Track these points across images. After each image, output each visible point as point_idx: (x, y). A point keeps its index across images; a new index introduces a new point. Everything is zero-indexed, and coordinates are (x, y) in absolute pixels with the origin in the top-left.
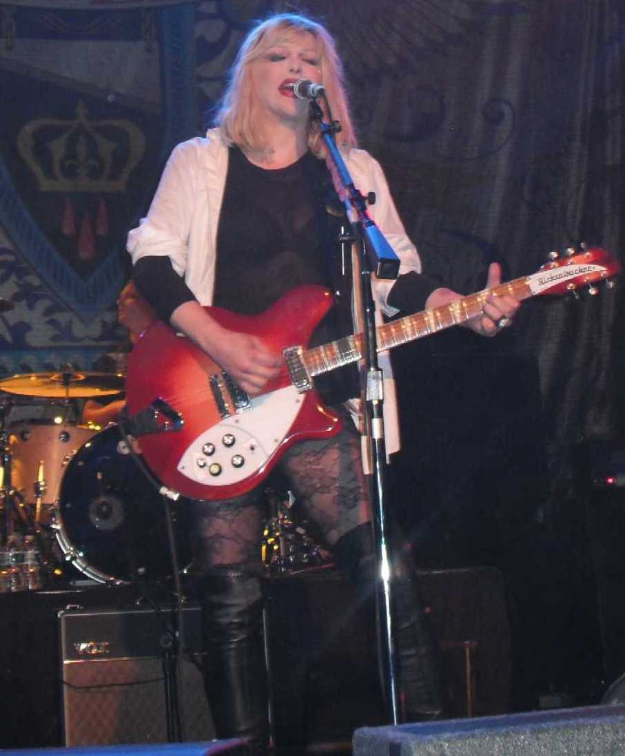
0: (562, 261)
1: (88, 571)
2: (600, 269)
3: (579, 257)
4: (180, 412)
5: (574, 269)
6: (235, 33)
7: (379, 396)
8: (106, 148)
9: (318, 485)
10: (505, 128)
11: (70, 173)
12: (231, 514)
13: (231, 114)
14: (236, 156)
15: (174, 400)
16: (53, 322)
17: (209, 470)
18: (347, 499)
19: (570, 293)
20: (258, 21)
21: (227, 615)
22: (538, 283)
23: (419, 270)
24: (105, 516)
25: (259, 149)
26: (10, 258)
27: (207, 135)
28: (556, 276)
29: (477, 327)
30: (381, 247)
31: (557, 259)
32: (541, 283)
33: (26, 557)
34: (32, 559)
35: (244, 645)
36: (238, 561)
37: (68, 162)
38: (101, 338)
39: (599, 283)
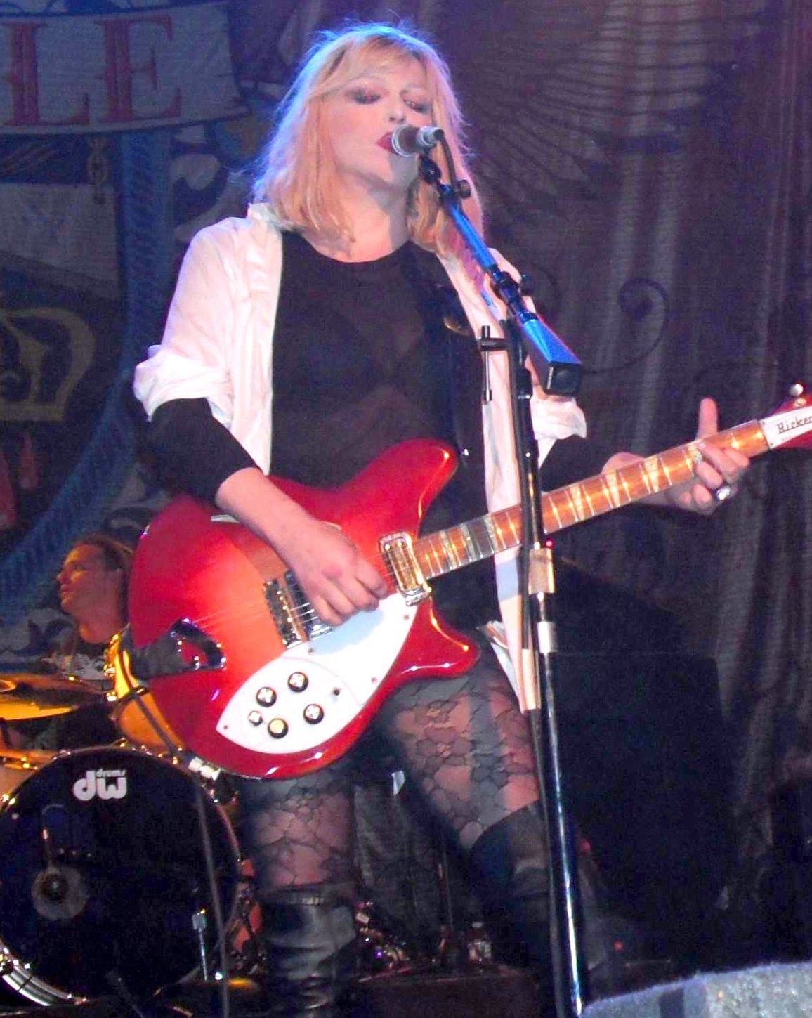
1: (27, 990)
6: (235, 176)
7: (547, 587)
8: (32, 351)
9: (446, 754)
10: (655, 321)
12: (306, 805)
13: (287, 178)
15: (214, 619)
17: (269, 728)
20: (328, 33)
21: (304, 965)
23: (583, 433)
24: (56, 898)
25: (332, 235)
27: (250, 212)
28: (805, 420)
29: (685, 500)
30: (550, 347)
32: (782, 430)
36: (320, 879)
38: (28, 651)
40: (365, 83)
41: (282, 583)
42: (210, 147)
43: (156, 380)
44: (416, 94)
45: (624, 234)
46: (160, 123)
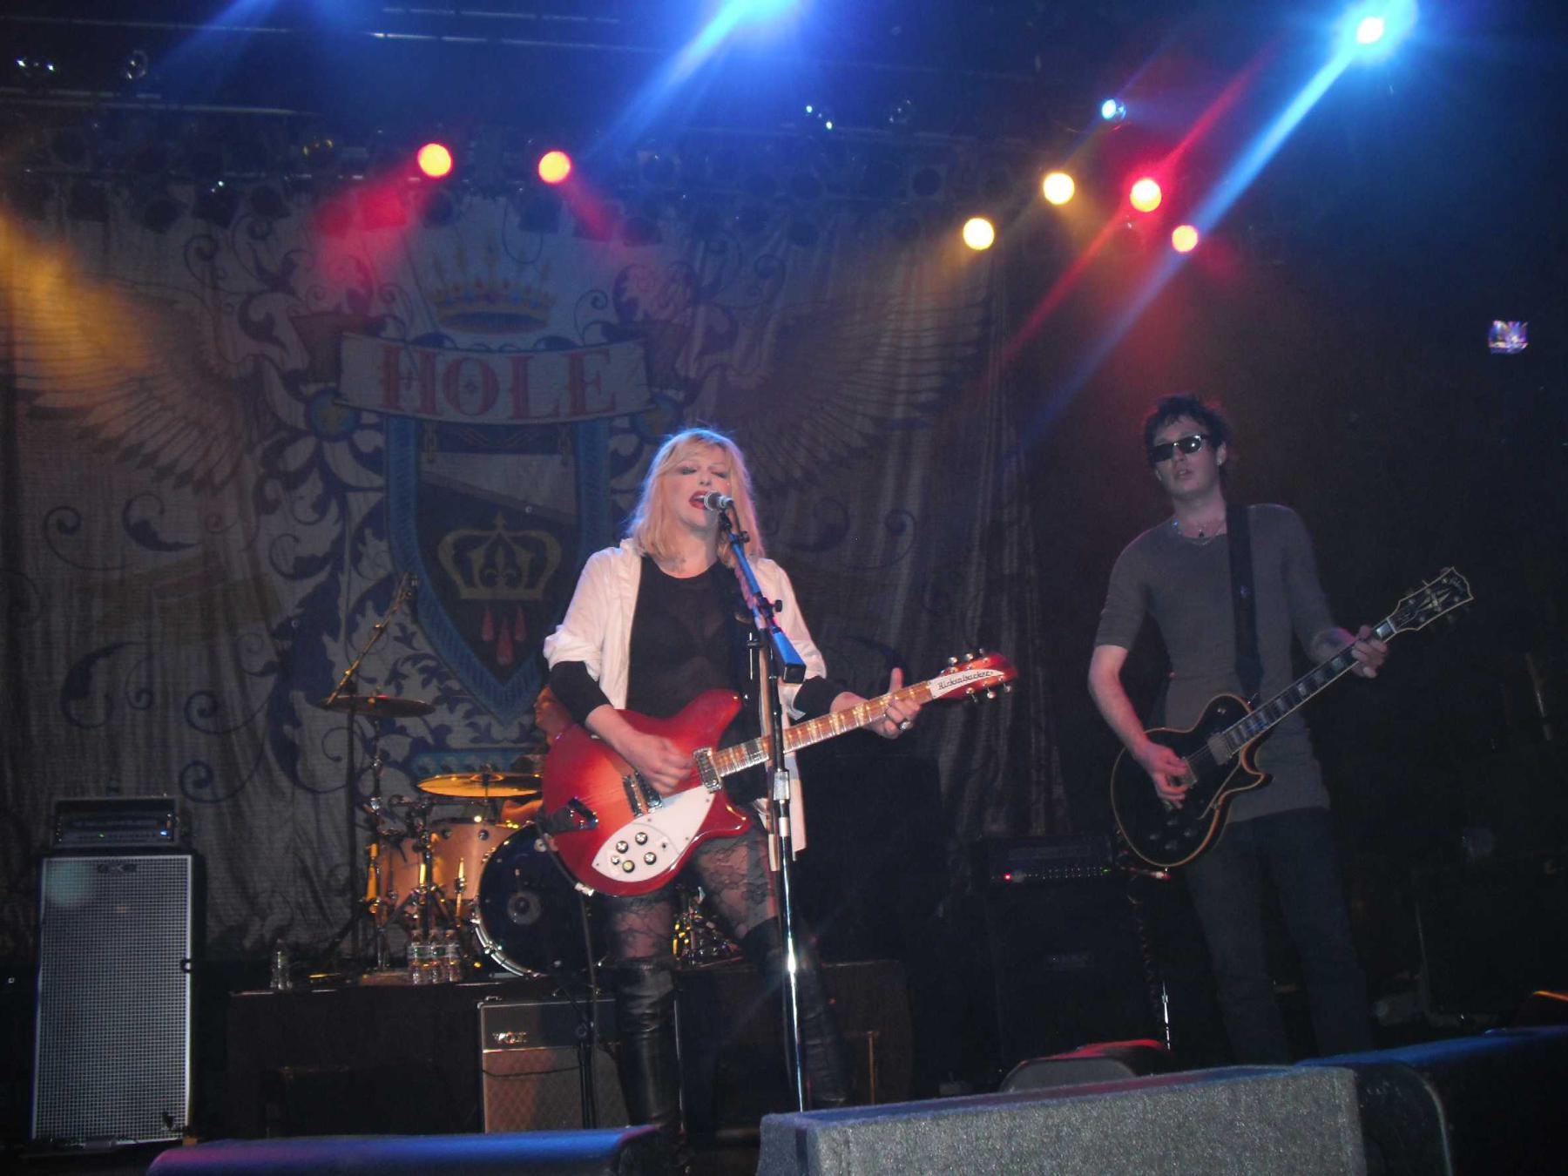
0: (961, 665)
2: (998, 674)
3: (978, 662)
6: (647, 448)
8: (524, 557)
9: (727, 882)
11: (489, 581)
15: (589, 799)
16: (472, 725)
19: (969, 697)
21: (640, 1006)
22: (938, 687)
23: (824, 675)
24: (523, 911)
26: (431, 663)
29: (880, 729)
30: (787, 653)
31: (956, 665)
32: (942, 687)
39: (996, 687)
40: (688, 464)
41: (634, 778)
42: (633, 429)
43: (555, 648)
44: (720, 468)
45: (890, 483)
46: (605, 415)
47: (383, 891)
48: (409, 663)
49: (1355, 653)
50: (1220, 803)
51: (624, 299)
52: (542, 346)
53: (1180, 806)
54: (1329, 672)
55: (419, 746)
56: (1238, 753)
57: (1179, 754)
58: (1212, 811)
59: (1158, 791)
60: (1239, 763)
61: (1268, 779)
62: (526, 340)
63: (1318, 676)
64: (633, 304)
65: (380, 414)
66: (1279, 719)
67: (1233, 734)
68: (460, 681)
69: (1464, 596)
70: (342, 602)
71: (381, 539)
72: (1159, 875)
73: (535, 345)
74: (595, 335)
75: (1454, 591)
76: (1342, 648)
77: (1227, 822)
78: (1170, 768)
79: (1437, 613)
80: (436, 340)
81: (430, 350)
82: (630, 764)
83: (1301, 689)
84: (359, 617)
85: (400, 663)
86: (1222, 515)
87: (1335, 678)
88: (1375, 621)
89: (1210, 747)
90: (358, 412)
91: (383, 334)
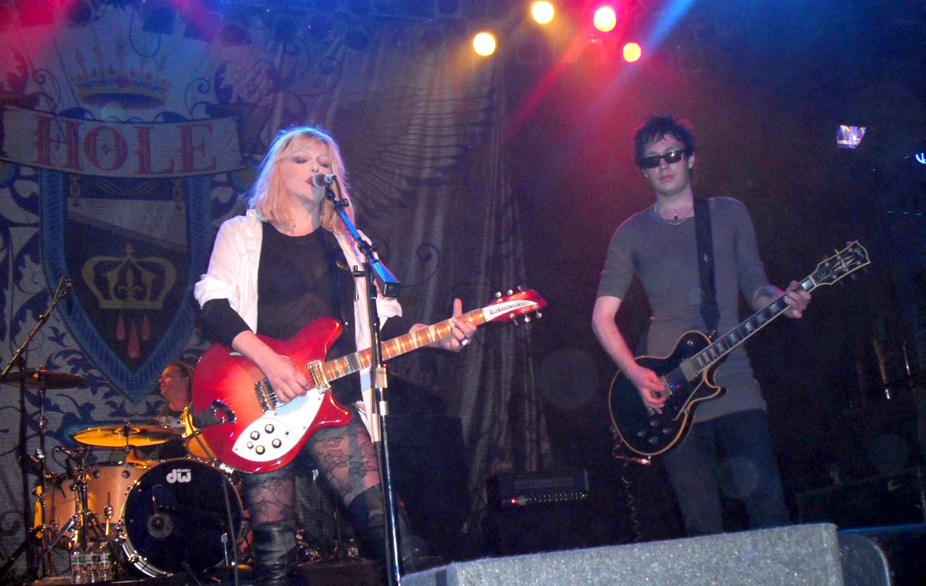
0: (505, 297)
2: (533, 304)
3: (517, 295)
4: (234, 410)
5: (514, 304)
6: (240, 197)
8: (148, 277)
9: (338, 462)
10: (433, 264)
11: (122, 296)
12: (273, 485)
13: (264, 198)
14: (268, 229)
15: (231, 400)
16: (112, 404)
17: (256, 450)
18: (358, 471)
19: (511, 321)
20: (284, 131)
21: (272, 559)
22: (490, 313)
23: (400, 315)
24: (159, 528)
25: (285, 224)
26: (79, 357)
28: (502, 308)
29: (447, 345)
31: (501, 297)
32: (491, 313)
33: (101, 558)
34: (106, 559)
35: (284, 581)
37: (120, 288)
38: (146, 415)
39: (532, 314)
40: (300, 154)
41: (262, 384)
42: (229, 183)
43: (204, 290)
44: (324, 159)
46: (206, 172)
47: (48, 519)
48: (61, 357)
49: (787, 300)
50: (689, 408)
51: (222, 86)
52: (160, 119)
53: (660, 412)
54: (768, 314)
55: (69, 420)
56: (702, 372)
57: (659, 374)
58: (683, 414)
59: (645, 401)
60: (703, 380)
61: (723, 391)
62: (148, 114)
63: (760, 318)
64: (229, 90)
65: (35, 168)
66: (732, 348)
67: (699, 359)
68: (100, 370)
69: (864, 261)
70: (7, 311)
71: (37, 263)
72: (644, 461)
73: (156, 118)
74: (201, 112)
75: (857, 257)
76: (775, 298)
77: (693, 422)
78: (653, 385)
79: (845, 272)
80: (78, 113)
81: (72, 120)
82: (260, 369)
83: (748, 326)
84: (20, 322)
85: (53, 356)
86: (690, 204)
87: (772, 319)
88: (801, 277)
89: (682, 369)
90: (18, 166)
91: (37, 108)
